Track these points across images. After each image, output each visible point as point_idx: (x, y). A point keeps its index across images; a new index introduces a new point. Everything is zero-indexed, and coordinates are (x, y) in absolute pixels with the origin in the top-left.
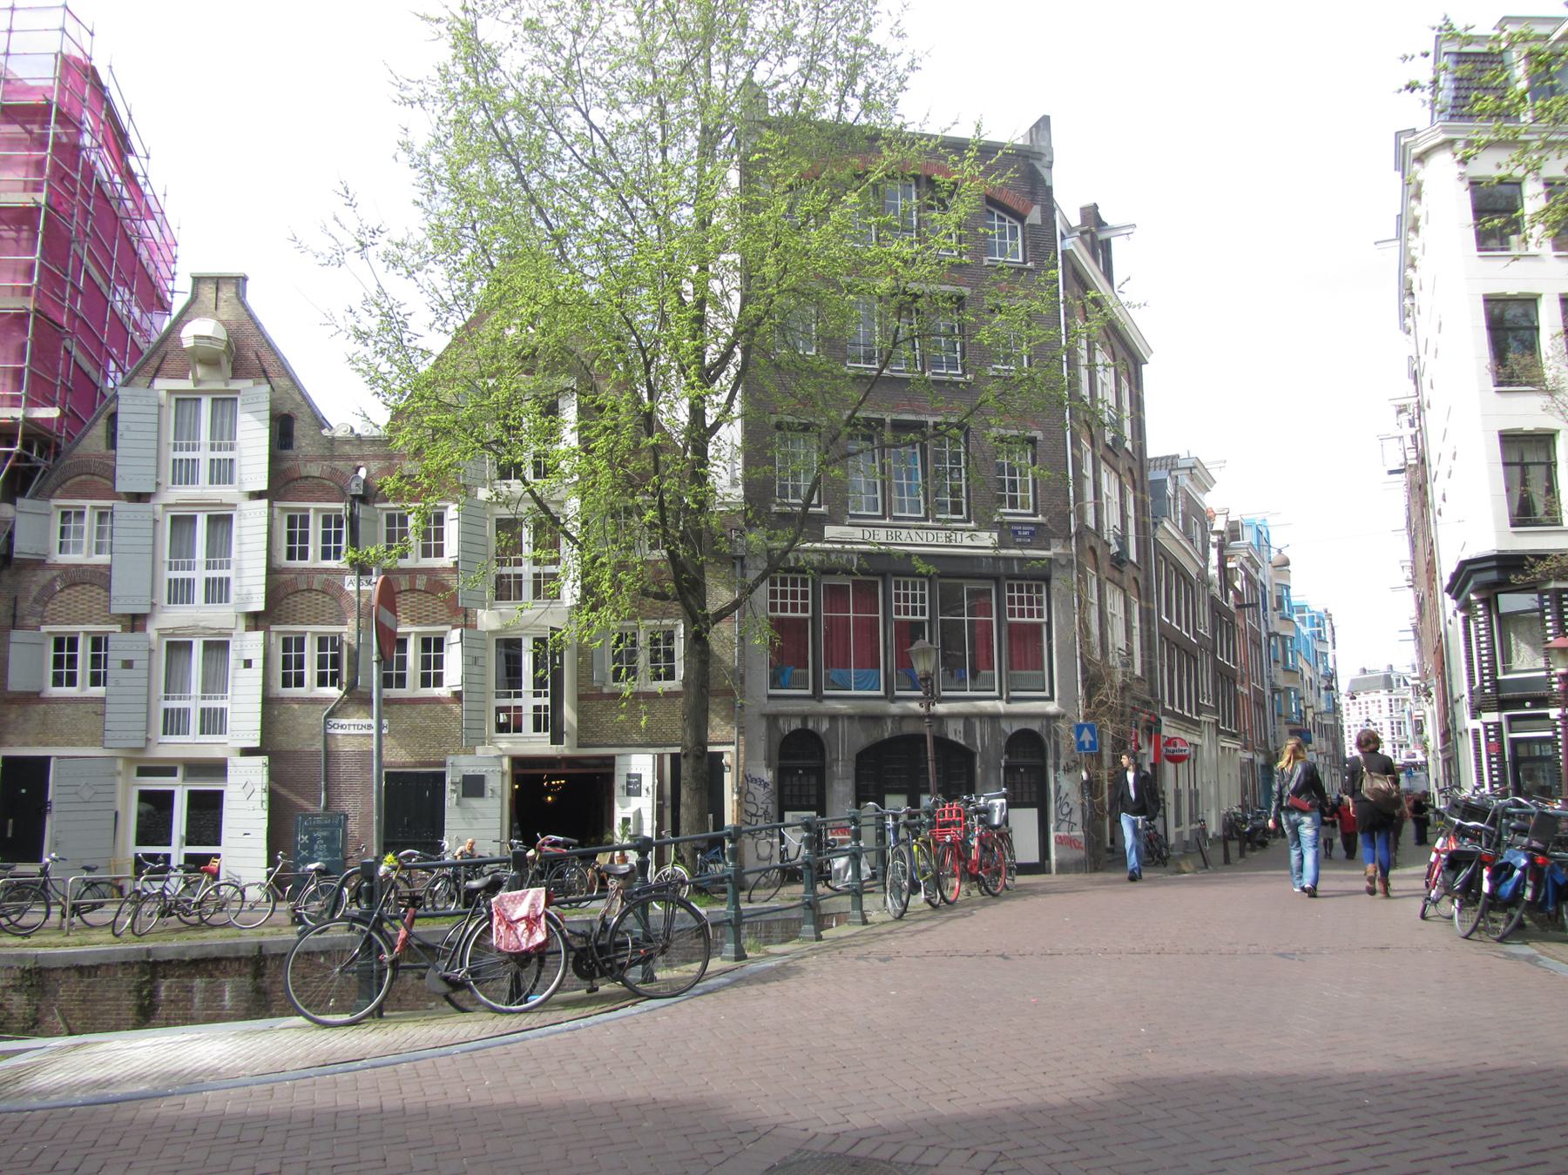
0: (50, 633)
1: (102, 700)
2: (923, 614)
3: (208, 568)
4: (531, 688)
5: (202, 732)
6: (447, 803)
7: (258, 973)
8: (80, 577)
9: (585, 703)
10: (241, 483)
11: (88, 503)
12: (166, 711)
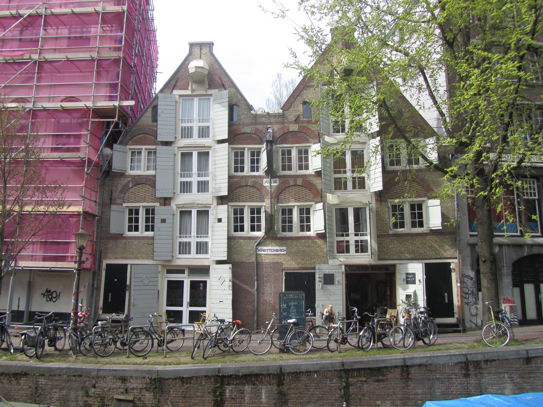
0: (127, 207)
1: (153, 238)
2: (535, 196)
3: (199, 176)
4: (353, 232)
5: (197, 253)
6: (317, 287)
7: (280, 383)
8: (139, 181)
9: (381, 239)
10: (214, 136)
11: (144, 147)
12: (180, 243)
